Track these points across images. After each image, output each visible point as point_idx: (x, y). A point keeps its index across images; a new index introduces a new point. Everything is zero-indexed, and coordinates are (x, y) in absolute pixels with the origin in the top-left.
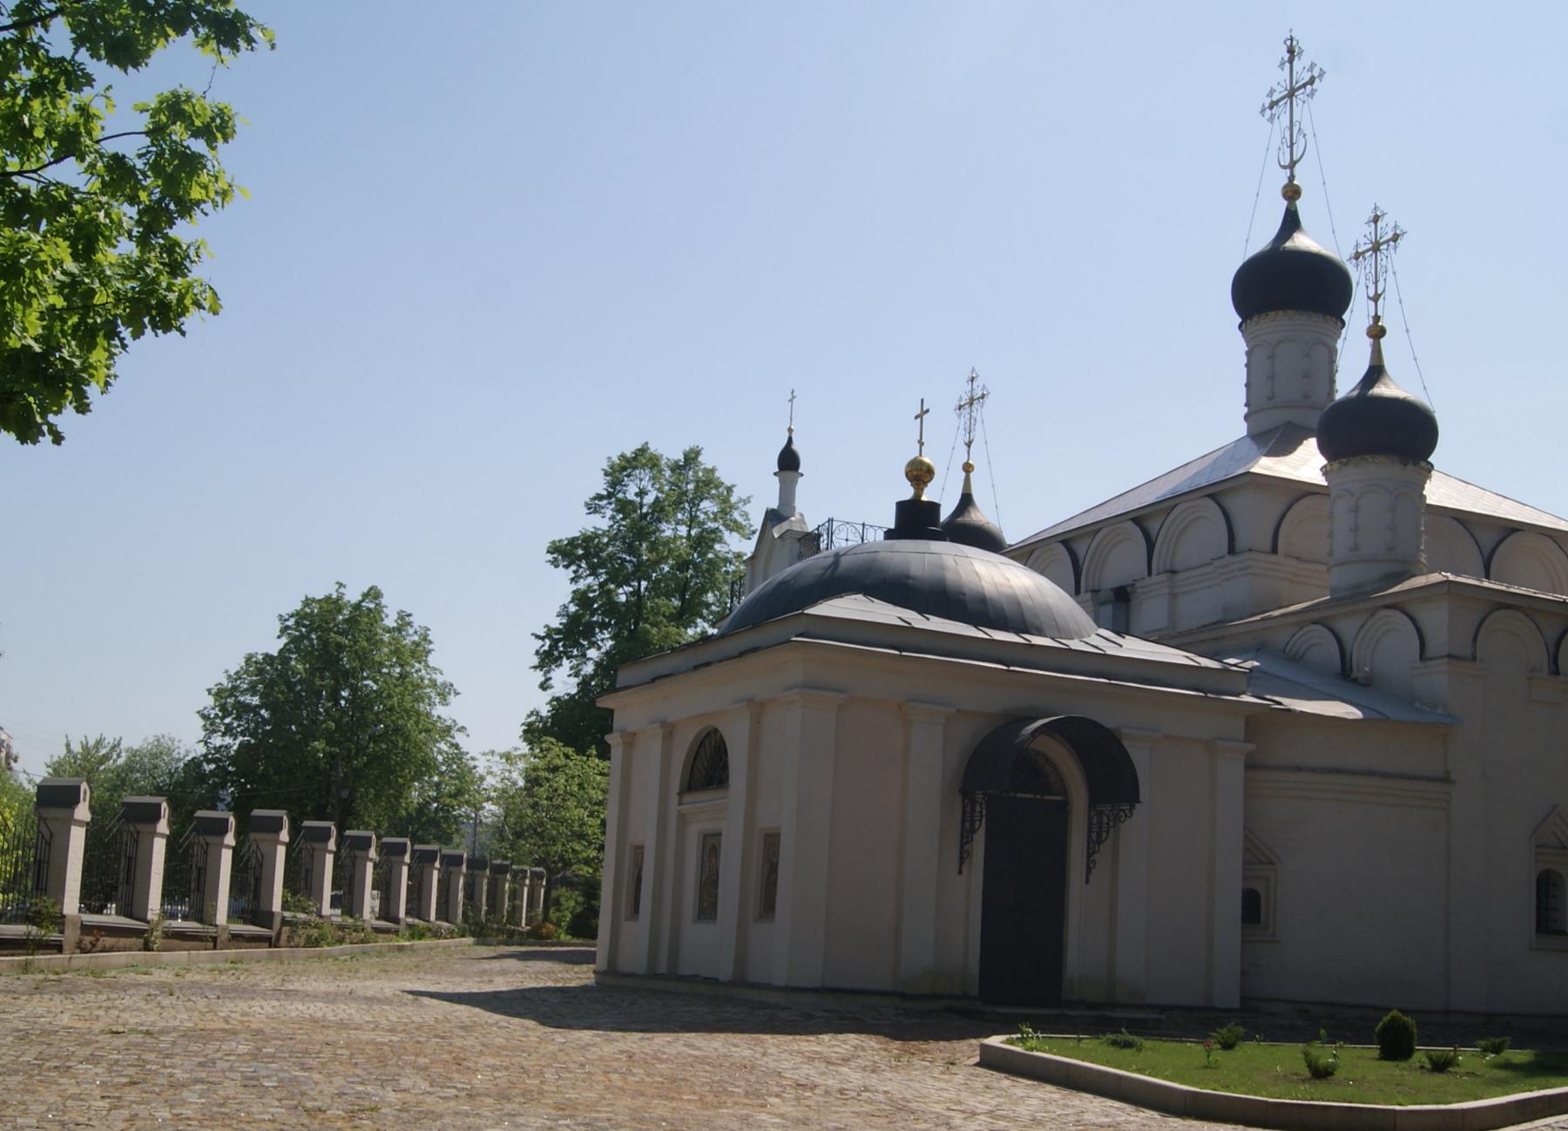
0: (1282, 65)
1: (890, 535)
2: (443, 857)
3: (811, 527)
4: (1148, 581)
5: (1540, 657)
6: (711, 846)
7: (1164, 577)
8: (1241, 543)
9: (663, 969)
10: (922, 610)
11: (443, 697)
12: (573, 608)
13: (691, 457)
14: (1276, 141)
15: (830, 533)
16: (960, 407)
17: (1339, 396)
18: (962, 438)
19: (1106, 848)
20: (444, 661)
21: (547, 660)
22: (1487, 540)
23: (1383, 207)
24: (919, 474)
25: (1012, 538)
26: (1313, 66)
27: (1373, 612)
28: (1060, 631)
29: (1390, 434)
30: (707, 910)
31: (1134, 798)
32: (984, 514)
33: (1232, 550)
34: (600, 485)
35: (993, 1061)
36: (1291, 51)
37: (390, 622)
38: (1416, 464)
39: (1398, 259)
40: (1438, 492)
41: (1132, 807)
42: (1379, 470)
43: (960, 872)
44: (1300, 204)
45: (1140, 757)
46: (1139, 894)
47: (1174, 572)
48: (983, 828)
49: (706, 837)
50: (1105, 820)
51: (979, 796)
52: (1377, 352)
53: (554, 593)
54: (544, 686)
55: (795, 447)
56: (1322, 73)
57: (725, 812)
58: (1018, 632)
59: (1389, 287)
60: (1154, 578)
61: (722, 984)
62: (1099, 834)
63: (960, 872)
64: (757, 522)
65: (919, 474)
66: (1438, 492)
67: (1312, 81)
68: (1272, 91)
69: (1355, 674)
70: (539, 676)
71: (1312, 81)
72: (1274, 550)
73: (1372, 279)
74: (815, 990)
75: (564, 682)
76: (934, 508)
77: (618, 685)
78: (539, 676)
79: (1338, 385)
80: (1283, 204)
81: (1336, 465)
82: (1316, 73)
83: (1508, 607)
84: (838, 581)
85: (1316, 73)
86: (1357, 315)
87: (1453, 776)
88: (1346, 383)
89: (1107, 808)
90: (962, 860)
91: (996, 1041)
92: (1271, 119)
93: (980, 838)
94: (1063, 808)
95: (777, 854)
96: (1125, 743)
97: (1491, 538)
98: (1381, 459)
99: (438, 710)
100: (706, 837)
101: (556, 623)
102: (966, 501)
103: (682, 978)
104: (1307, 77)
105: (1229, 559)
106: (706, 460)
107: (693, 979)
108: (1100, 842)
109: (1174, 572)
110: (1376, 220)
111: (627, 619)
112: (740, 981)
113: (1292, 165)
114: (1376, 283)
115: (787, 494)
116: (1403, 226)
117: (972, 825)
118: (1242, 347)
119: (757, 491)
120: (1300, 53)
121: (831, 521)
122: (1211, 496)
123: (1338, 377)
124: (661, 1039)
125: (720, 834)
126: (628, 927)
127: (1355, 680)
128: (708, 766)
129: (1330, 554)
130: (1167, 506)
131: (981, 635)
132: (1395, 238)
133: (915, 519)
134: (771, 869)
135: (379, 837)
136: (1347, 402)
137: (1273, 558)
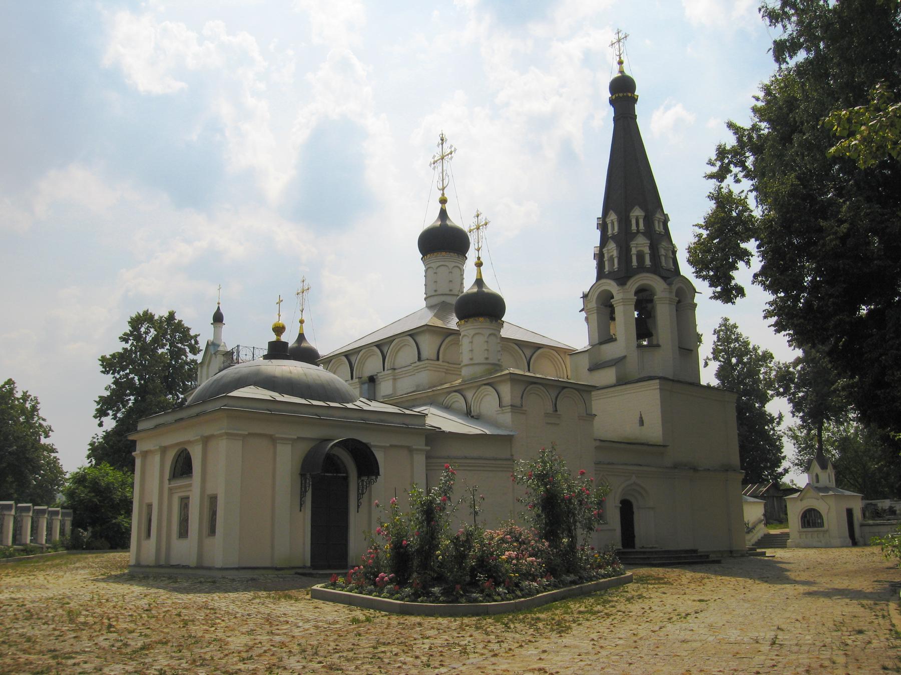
0: (438, 145)
1: (266, 357)
2: (49, 512)
3: (229, 349)
4: (383, 373)
5: (550, 409)
6: (185, 503)
7: (390, 372)
9: (162, 562)
10: (281, 393)
11: (47, 436)
12: (113, 386)
13: (172, 315)
14: (436, 178)
17: (465, 291)
19: (366, 496)
20: (47, 414)
21: (101, 413)
22: (528, 352)
23: (480, 211)
24: (279, 330)
25: (324, 351)
26: (451, 146)
27: (479, 387)
28: (344, 398)
29: (485, 308)
30: (183, 533)
31: (377, 473)
32: (312, 342)
33: (419, 359)
34: (128, 329)
35: (316, 595)
36: (442, 140)
37: (19, 395)
38: (496, 321)
39: (483, 232)
40: (505, 333)
41: (377, 478)
44: (448, 207)
45: (380, 456)
46: (379, 517)
50: (345, 654)
51: (308, 476)
53: (103, 384)
54: (101, 425)
55: (222, 311)
56: (455, 150)
57: (194, 487)
58: (324, 401)
59: (483, 244)
60: (386, 372)
61: (191, 568)
64: (202, 345)
65: (279, 330)
66: (505, 333)
67: (451, 153)
68: (434, 156)
69: (473, 414)
70: (97, 421)
71: (451, 153)
72: (438, 359)
74: (237, 569)
75: (110, 423)
76: (286, 344)
78: (97, 421)
79: (465, 285)
80: (439, 206)
81: (463, 322)
83: (535, 383)
86: (471, 255)
88: (468, 285)
89: (365, 478)
90: (301, 505)
91: (317, 587)
92: (434, 169)
94: (346, 479)
95: (216, 506)
96: (373, 449)
97: (531, 350)
98: (481, 319)
99: (43, 441)
101: (107, 393)
102: (301, 337)
103: (173, 566)
105: (418, 363)
106: (178, 317)
107: (177, 567)
111: (141, 392)
112: (199, 567)
113: (443, 189)
115: (217, 334)
116: (489, 219)
117: (305, 488)
121: (238, 346)
122: (410, 335)
123: (465, 281)
126: (145, 543)
127: (472, 417)
128: (183, 466)
130: (390, 340)
133: (277, 350)
134: (213, 514)
135: (16, 504)
137: (437, 363)
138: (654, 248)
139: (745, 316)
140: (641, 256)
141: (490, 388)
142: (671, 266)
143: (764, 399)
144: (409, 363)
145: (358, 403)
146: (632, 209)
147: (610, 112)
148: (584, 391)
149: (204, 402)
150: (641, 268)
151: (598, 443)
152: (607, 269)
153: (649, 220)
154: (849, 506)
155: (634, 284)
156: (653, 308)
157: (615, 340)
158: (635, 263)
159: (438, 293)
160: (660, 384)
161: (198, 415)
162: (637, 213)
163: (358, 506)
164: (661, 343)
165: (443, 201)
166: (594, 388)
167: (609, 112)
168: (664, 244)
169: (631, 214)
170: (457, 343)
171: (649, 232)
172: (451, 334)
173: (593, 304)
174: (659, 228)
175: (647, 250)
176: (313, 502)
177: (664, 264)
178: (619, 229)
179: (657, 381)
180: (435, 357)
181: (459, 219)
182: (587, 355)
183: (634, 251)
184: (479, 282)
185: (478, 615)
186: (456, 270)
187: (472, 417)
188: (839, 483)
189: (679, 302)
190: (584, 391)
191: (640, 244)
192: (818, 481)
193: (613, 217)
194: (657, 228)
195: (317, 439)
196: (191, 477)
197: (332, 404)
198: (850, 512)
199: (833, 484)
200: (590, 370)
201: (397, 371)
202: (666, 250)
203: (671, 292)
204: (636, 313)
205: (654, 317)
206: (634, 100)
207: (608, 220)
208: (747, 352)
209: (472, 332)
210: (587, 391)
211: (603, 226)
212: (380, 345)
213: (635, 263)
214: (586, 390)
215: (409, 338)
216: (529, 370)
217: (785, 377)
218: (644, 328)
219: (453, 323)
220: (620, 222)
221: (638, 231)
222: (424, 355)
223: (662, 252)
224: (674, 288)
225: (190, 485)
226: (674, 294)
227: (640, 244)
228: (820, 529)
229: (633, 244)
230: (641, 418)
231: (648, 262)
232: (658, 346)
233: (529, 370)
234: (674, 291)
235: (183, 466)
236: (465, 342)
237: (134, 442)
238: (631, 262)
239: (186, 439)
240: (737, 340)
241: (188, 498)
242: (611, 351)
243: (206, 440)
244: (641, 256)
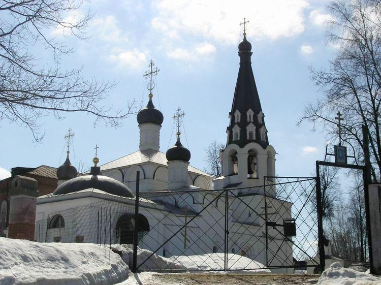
8: (146, 177)
18: (66, 145)
31: (148, 230)
33: (145, 178)
36: (152, 64)
40: (190, 169)
42: (178, 164)
52: (179, 137)
67: (157, 71)
68: (146, 72)
71: (157, 71)
72: (154, 179)
77: (269, 227)
80: (149, 98)
83: (112, 200)
98: (176, 161)
105: (144, 180)
110: (179, 110)
113: (151, 89)
118: (139, 130)
120: (154, 64)
129: (169, 180)
131: (147, 201)
132: (183, 114)
147: (238, 59)
150: (251, 141)
152: (234, 140)
153: (255, 117)
155: (249, 146)
158: (248, 138)
164: (259, 177)
167: (238, 59)
174: (260, 121)
177: (262, 139)
180: (152, 178)
193: (238, 114)
206: (251, 54)
207: (236, 115)
211: (232, 114)
227: (251, 128)
229: (248, 128)
238: (247, 136)
244: (251, 134)
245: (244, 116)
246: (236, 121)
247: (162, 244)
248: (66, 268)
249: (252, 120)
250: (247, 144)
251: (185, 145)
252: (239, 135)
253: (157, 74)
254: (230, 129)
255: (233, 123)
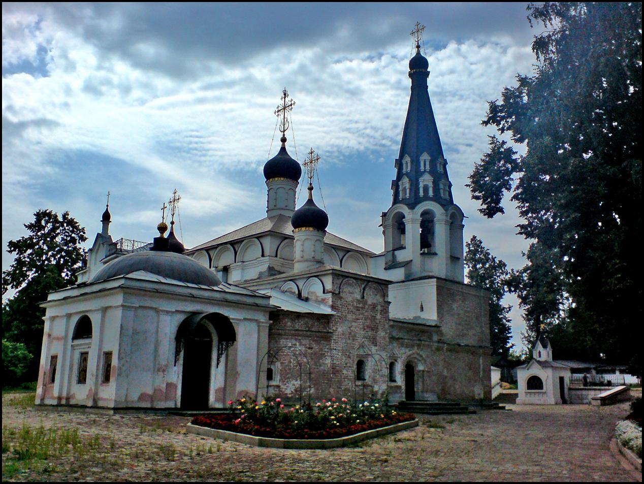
0: (282, 99)
4: (234, 264)
6: (84, 357)
7: (240, 263)
15: (122, 243)
16: (170, 202)
17: (298, 207)
29: (314, 219)
30: (82, 379)
33: (263, 255)
36: (285, 94)
40: (326, 240)
41: (233, 343)
43: (175, 365)
47: (244, 262)
48: (183, 351)
49: (82, 354)
57: (93, 347)
58: (196, 284)
60: (237, 264)
62: (222, 351)
63: (175, 365)
67: (291, 105)
68: (278, 107)
71: (291, 105)
72: (276, 256)
73: (310, 171)
82: (293, 102)
84: (135, 266)
85: (293, 102)
87: (524, 394)
92: (278, 116)
93: (182, 354)
94: (211, 341)
97: (346, 251)
100: (82, 354)
104: (290, 103)
105: (262, 258)
108: (222, 354)
109: (244, 262)
113: (284, 131)
114: (311, 173)
115: (105, 228)
119: (91, 227)
120: (288, 95)
121: (122, 239)
124: (182, 374)
125: (57, 356)
128: (83, 329)
130: (240, 241)
136: (299, 210)
138: (436, 184)
139: (506, 238)
140: (426, 189)
141: (316, 279)
142: (447, 197)
143: (500, 295)
144: (255, 258)
145: (221, 286)
146: (422, 153)
148: (322, 275)
149: (105, 281)
150: (426, 198)
151: (392, 323)
152: (400, 198)
153: (433, 163)
154: (562, 375)
155: (420, 208)
156: (433, 226)
157: (405, 248)
158: (421, 193)
159: (287, 208)
160: (437, 282)
161: (100, 291)
162: (425, 157)
163: (218, 364)
165: (284, 140)
166: (391, 282)
168: (443, 181)
169: (421, 158)
170: (292, 245)
171: (433, 172)
172: (286, 238)
173: (390, 222)
174: (440, 169)
175: (430, 185)
176: (184, 357)
178: (411, 167)
179: (435, 279)
180: (274, 254)
181: (297, 154)
182: (383, 258)
183: (421, 185)
184: (310, 201)
185: (311, 448)
186: (291, 192)
187: (302, 300)
188: (555, 358)
189: (452, 223)
190: (322, 275)
191: (426, 180)
192: (540, 356)
194: (438, 169)
195: (191, 312)
196: (91, 337)
197: (203, 287)
198: (562, 379)
199: (550, 359)
200: (385, 269)
201: (245, 263)
202: (445, 185)
203: (447, 216)
204: (421, 229)
205: (433, 233)
206: (428, 74)
207: (404, 162)
208: (487, 260)
209: (304, 238)
210: (385, 284)
211: (399, 164)
212: (233, 243)
213: (421, 193)
214: (383, 285)
215: (256, 240)
216: (341, 267)
217: (514, 283)
218: (426, 241)
219: (289, 229)
220: (412, 162)
221: (425, 171)
222: (267, 252)
223: (441, 186)
224: (450, 212)
225: (90, 343)
226: (449, 217)
228: (540, 391)
229: (421, 179)
230: (422, 306)
231: (431, 193)
232: (436, 254)
233: (341, 267)
234: (449, 215)
235: (83, 329)
236: (298, 246)
237: (44, 310)
239: (87, 309)
240: (482, 252)
241: (87, 353)
242: (401, 256)
243: (105, 310)
244: (426, 189)
245: (416, 162)
246: (404, 171)
247: (261, 373)
248: (567, 211)
249: (428, 168)
250: (419, 204)
251: (319, 204)
252: (408, 191)
253: (292, 108)
254: (396, 185)
255: (400, 176)
